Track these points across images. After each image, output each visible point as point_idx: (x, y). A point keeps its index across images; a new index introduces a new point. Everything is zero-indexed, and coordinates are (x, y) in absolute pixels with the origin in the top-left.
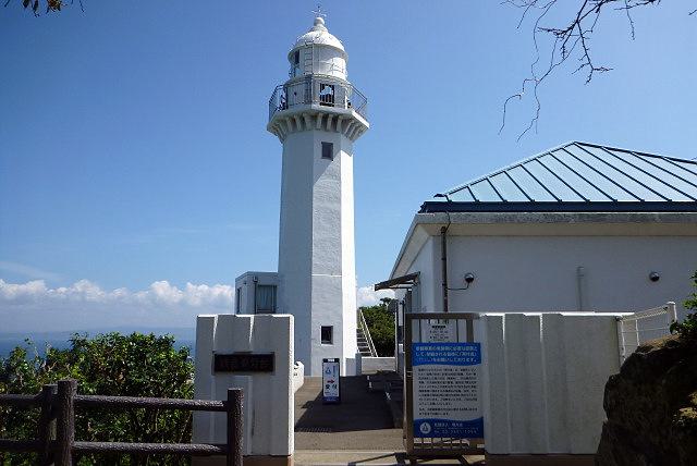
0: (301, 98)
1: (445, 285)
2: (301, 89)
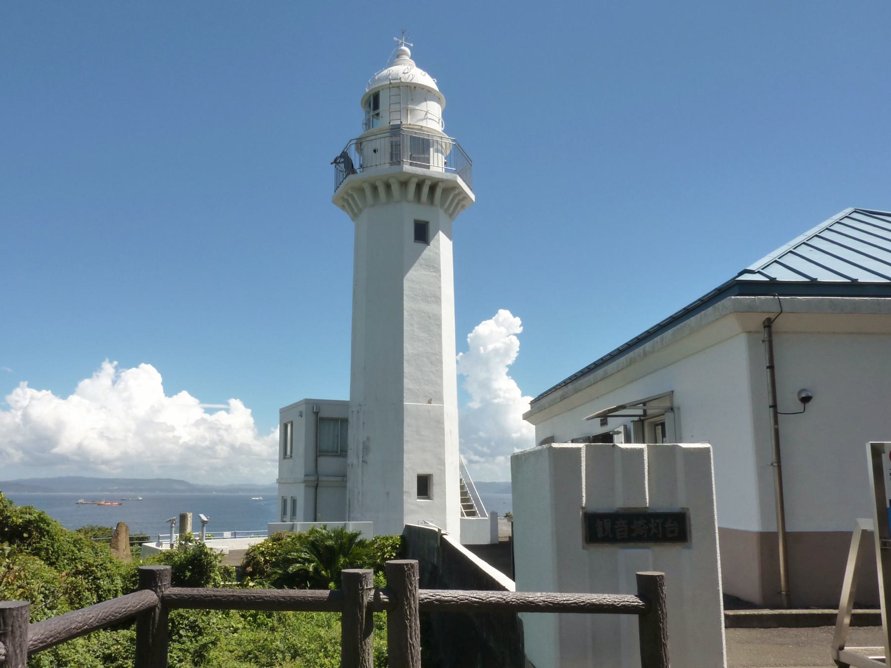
0: (384, 157)
1: (774, 406)
2: (384, 145)
